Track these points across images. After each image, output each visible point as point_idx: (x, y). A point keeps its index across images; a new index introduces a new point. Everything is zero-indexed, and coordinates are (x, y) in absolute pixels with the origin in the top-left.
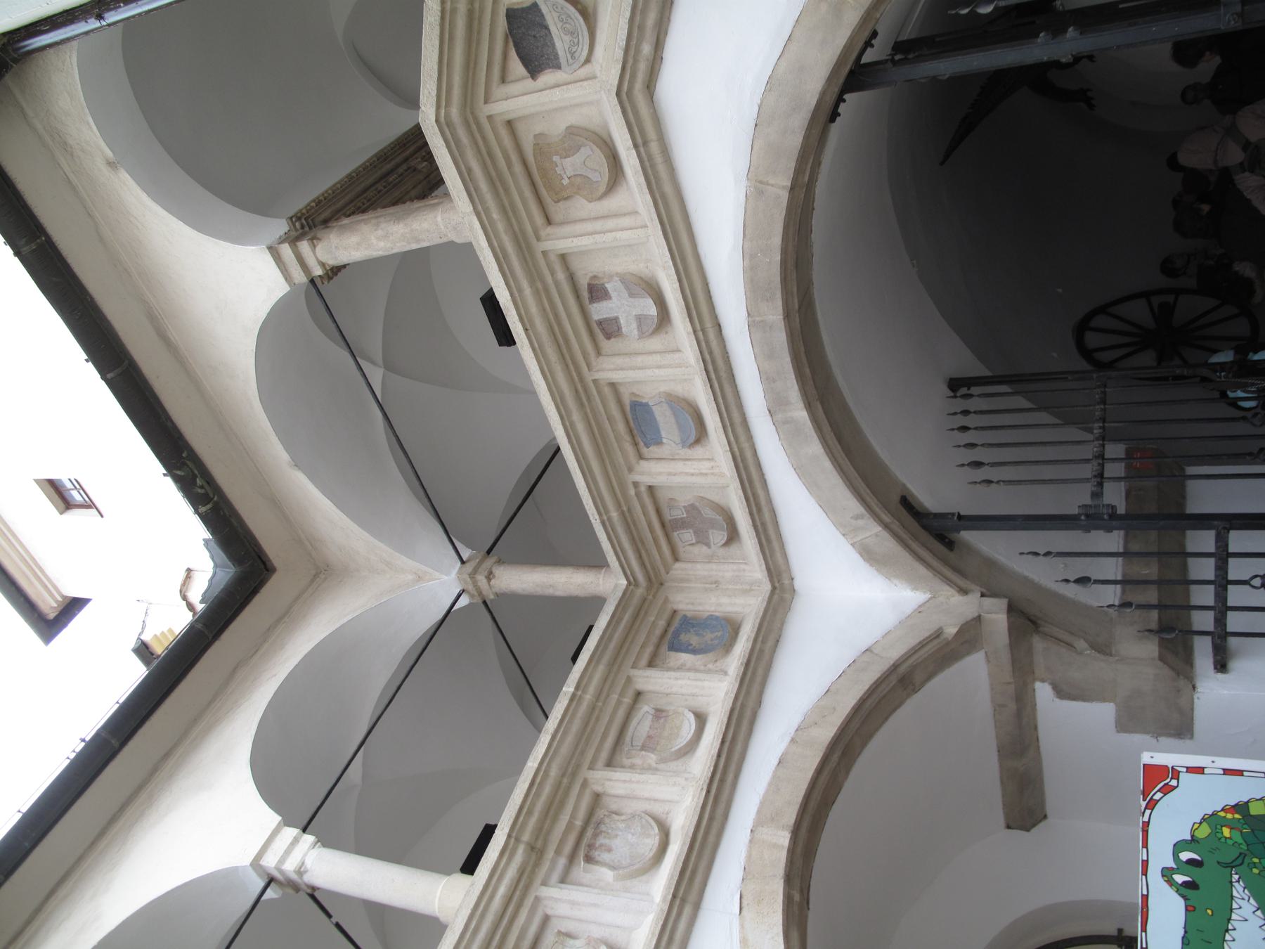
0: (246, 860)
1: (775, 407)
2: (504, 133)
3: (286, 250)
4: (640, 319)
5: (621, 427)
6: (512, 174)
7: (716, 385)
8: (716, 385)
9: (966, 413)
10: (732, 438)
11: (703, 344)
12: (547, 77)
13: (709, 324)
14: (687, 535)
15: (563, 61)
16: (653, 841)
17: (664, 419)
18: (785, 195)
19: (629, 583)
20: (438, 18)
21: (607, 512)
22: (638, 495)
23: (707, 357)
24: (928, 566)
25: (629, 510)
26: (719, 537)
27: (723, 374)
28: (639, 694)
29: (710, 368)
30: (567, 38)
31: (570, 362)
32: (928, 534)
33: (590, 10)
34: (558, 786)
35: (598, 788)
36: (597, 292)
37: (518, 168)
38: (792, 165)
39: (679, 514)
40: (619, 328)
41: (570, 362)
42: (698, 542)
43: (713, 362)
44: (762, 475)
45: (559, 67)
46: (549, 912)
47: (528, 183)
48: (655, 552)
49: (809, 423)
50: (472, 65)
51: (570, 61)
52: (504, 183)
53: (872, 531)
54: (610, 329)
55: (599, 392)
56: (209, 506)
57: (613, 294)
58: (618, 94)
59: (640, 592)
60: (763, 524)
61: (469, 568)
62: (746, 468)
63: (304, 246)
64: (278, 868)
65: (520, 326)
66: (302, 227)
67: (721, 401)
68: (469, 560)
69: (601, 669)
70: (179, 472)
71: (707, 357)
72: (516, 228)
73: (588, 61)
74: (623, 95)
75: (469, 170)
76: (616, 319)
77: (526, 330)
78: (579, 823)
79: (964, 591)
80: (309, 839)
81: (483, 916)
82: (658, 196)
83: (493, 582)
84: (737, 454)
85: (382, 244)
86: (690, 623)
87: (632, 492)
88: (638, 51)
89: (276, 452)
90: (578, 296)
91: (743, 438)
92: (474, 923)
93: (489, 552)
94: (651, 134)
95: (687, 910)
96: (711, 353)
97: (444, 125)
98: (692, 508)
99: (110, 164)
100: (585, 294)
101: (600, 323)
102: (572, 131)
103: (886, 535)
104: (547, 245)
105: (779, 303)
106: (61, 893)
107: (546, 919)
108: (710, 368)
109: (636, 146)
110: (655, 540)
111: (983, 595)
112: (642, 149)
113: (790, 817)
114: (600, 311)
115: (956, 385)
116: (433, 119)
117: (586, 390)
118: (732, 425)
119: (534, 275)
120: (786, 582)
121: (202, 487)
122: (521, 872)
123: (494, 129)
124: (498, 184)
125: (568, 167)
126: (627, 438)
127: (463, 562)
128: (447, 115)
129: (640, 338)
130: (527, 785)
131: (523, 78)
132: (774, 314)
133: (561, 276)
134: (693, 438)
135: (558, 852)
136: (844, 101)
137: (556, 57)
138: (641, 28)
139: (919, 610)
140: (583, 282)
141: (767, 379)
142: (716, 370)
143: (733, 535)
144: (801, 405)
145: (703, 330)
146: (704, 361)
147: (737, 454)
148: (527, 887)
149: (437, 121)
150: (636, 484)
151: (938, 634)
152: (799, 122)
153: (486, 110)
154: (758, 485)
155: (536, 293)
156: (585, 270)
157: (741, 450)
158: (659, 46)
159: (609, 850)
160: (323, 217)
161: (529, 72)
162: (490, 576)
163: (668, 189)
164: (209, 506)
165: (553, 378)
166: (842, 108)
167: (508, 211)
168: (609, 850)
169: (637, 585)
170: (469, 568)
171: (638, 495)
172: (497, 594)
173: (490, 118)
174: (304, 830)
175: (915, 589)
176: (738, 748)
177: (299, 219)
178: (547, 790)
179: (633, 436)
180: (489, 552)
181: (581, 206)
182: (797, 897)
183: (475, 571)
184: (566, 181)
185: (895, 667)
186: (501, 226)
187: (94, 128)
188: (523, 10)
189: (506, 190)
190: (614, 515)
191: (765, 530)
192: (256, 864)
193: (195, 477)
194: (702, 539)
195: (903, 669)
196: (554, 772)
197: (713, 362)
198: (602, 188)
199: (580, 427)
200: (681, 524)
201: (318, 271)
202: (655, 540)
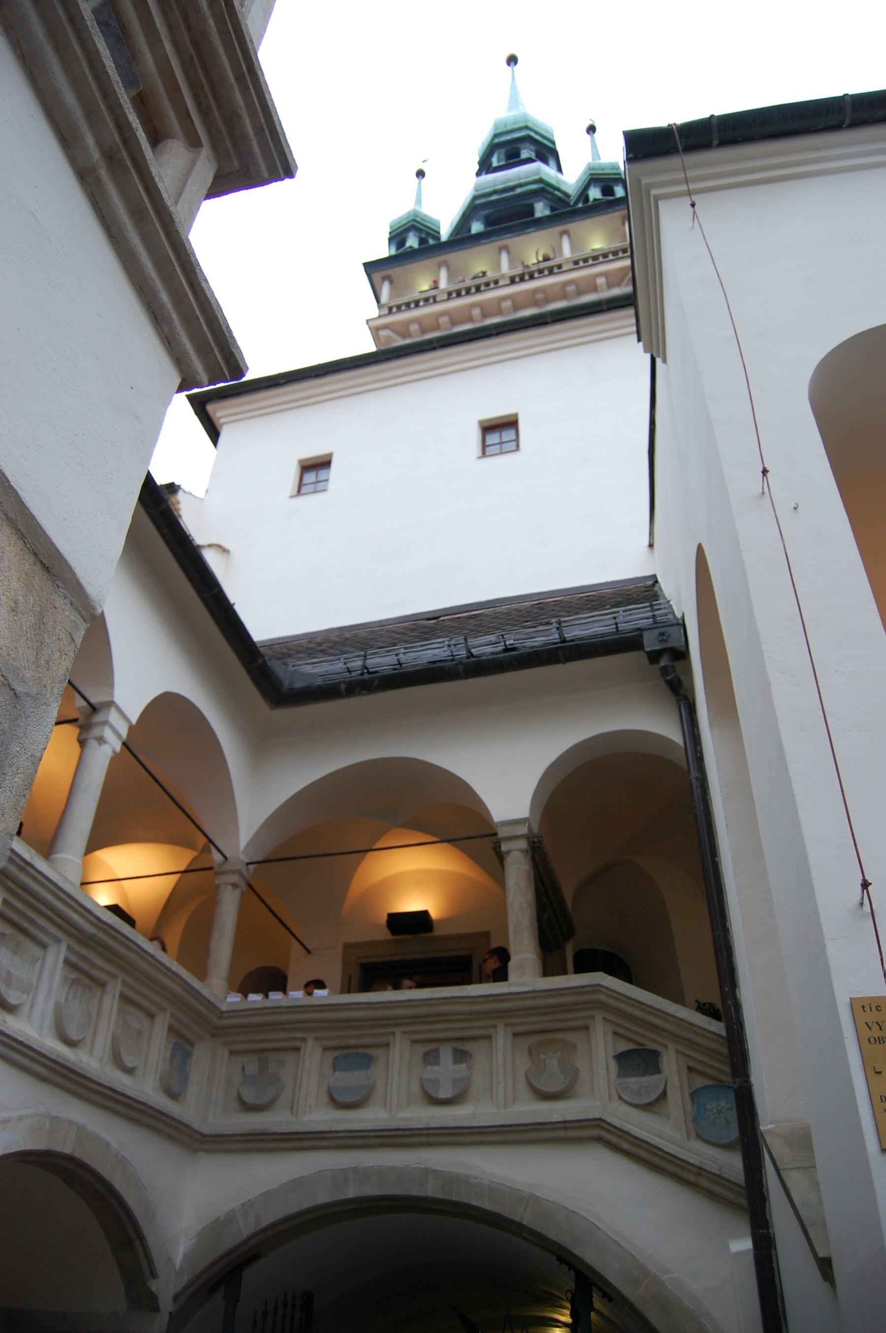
0: (117, 699)
1: (362, 1174)
2: (581, 1023)
3: (523, 830)
4: (436, 1082)
5: (353, 1042)
8: (385, 1133)
9: (294, 1306)
10: (341, 1135)
11: (419, 1132)
12: (613, 1066)
14: (252, 1068)
16: (73, 1033)
17: (355, 1078)
18: (517, 1218)
19: (222, 1012)
20: (663, 1009)
21: (287, 1013)
22: (296, 1039)
23: (408, 1133)
24: (204, 1271)
26: (249, 1096)
28: (152, 1016)
29: (399, 1133)
32: (228, 1272)
35: (109, 987)
36: (461, 1056)
37: (556, 1025)
38: (537, 1228)
43: (402, 1136)
45: (619, 1076)
46: (50, 949)
47: (545, 1028)
49: (343, 1197)
52: (548, 1014)
53: (246, 1228)
54: (431, 1058)
58: (600, 1119)
59: (214, 1019)
60: (262, 1141)
61: (243, 869)
63: (523, 844)
64: (105, 723)
65: (448, 995)
66: (534, 842)
67: (372, 1134)
68: (248, 869)
69: (177, 989)
70: (376, 682)
71: (408, 1133)
73: (620, 1098)
74: (599, 1122)
75: (563, 995)
76: (438, 1064)
77: (445, 998)
78: (94, 972)
79: (176, 1298)
80: (118, 746)
82: (529, 1127)
83: (230, 887)
86: (187, 1055)
88: (625, 1140)
90: (458, 1039)
92: (63, 896)
93: (249, 885)
94: (571, 1134)
95: (45, 1072)
97: (596, 988)
101: (437, 1050)
102: (576, 1072)
103: (239, 1240)
104: (501, 1030)
105: (440, 1196)
107: (44, 947)
108: (399, 1133)
109: (565, 1122)
110: (254, 1041)
111: (171, 1314)
112: (562, 1125)
113: (78, 1155)
114: (446, 1053)
115: (308, 1298)
116: (602, 983)
117: (388, 1025)
118: (351, 1137)
123: (585, 1018)
125: (552, 1061)
126: (343, 1043)
127: (248, 864)
128: (601, 992)
131: (615, 1048)
132: (431, 1190)
133: (476, 1032)
134: (337, 1097)
135: (82, 957)
136: (569, 1270)
137: (626, 1076)
138: (639, 1146)
139: (170, 1260)
140: (467, 1046)
142: (396, 1136)
143: (247, 1107)
145: (428, 1135)
146: (405, 1130)
148: (69, 934)
149: (599, 985)
150: (304, 1040)
151: (154, 1274)
152: (566, 1241)
153: (599, 1016)
156: (478, 1050)
159: (74, 997)
160: (537, 857)
161: (619, 1055)
162: (235, 886)
163: (532, 1135)
166: (565, 1267)
167: (529, 1011)
168: (74, 997)
169: (220, 1018)
170: (243, 869)
171: (296, 1039)
172: (218, 886)
173: (593, 1017)
174: (124, 744)
175: (185, 1255)
177: (540, 842)
178: (123, 951)
179: (342, 1048)
180: (249, 885)
181: (523, 1064)
182: (32, 1159)
183: (241, 874)
184: (542, 1057)
185: (141, 1237)
186: (521, 1004)
188: (658, 1062)
189: (544, 1014)
190: (284, 1018)
192: (111, 704)
195: (137, 1243)
196: (132, 956)
197: (402, 1136)
198: (535, 1083)
201: (504, 847)
202: (254, 1041)
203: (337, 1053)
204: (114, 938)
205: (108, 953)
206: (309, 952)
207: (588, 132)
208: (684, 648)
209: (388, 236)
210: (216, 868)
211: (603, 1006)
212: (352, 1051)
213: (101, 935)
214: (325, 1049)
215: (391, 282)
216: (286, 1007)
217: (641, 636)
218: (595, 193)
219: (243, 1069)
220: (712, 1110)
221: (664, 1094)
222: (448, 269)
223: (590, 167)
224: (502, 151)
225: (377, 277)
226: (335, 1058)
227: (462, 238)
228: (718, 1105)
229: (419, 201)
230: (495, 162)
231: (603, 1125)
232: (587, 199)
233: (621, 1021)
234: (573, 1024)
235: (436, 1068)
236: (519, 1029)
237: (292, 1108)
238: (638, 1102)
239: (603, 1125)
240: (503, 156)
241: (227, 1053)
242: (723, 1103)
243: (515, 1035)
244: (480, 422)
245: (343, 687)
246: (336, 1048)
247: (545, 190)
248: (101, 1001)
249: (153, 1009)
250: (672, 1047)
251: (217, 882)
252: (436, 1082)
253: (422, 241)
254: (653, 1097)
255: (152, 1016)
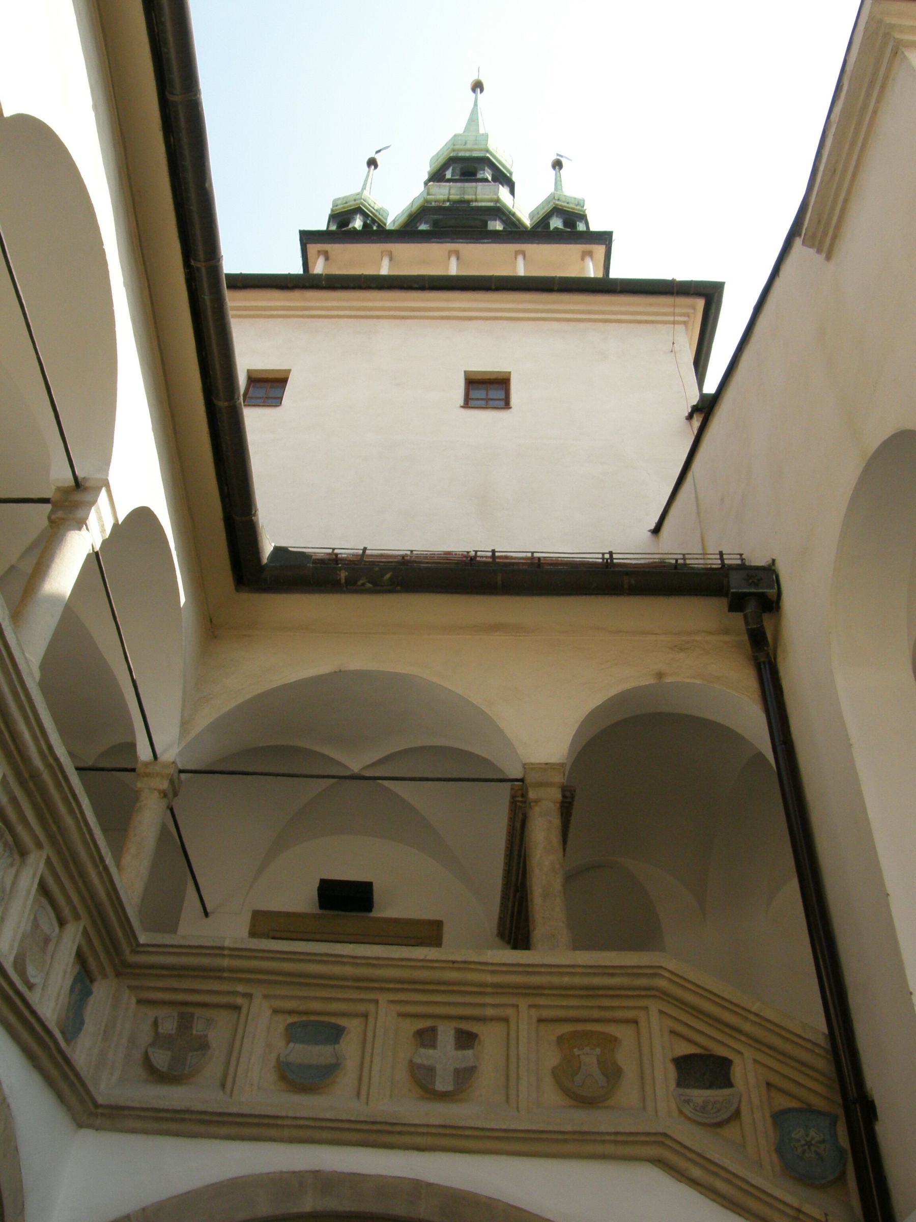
2: (630, 1014)
4: (431, 1070)
5: (316, 1006)
6: (592, 1007)
7: (364, 1127)
8: (364, 1127)
13: (429, 1141)
14: (169, 1026)
15: (681, 1091)
17: (315, 1054)
22: (235, 993)
23: (399, 1129)
25: (220, 978)
27: (372, 1137)
30: (700, 1101)
31: (405, 986)
33: (718, 1130)
34: (57, 820)
35: (32, 858)
37: (596, 1014)
39: (198, 1028)
40: (424, 1046)
41: (405, 986)
42: (157, 1033)
44: (242, 1138)
48: (160, 984)
49: (295, 1210)
50: (694, 1013)
51: (683, 1098)
55: (362, 1000)
56: (343, 581)
57: (460, 1053)
58: (665, 1135)
62: (258, 1125)
70: (388, 576)
72: (547, 992)
74: (662, 1138)
75: (612, 975)
81: (21, 708)
83: (156, 794)
84: (279, 1122)
85: (547, 863)
87: (240, 988)
89: (357, 659)
91: (296, 1133)
96: (400, 1133)
97: (655, 972)
98: (203, 1046)
99: (660, 675)
100: (465, 1026)
101: (433, 1029)
106: (146, 292)
114: (446, 1034)
116: (664, 965)
119: (500, 989)
120: (98, 1122)
121: (363, 585)
122: (25, 759)
124: (591, 993)
127: (181, 771)
129: (411, 1062)
130: (77, 792)
133: (489, 1012)
141: (354, 1180)
144: (319, 1208)
147: (279, 1122)
149: (661, 967)
153: (654, 1006)
154: (233, 1130)
155: (484, 985)
157: (282, 1127)
158: (694, 1183)
163: (570, 1148)
164: (343, 581)
165: (398, 966)
167: (565, 991)
169: (134, 952)
176: (25, 1035)
178: (62, 809)
184: (576, 1051)
187: (688, 680)
190: (226, 962)
191: (173, 1120)
193: (375, 584)
194: (158, 1040)
196: (69, 821)
199: (336, 970)
200: (185, 1022)
201: (532, 795)
202: (175, 990)
203: (290, 1019)
204: (58, 785)
205: (45, 810)
206: (206, 914)
207: (554, 167)
208: (775, 599)
209: (329, 212)
210: (140, 769)
211: (664, 995)
212: (312, 1018)
213: (46, 776)
214: (276, 1011)
215: (327, 259)
216: (230, 949)
217: (727, 576)
218: (556, 223)
219: (156, 1023)
220: (799, 1141)
221: (737, 1114)
222: (391, 259)
223: (552, 197)
224: (459, 167)
225: (312, 248)
226: (292, 1025)
227: (408, 232)
228: (807, 1135)
229: (364, 188)
230: (448, 175)
231: (668, 1142)
232: (548, 225)
233: (684, 1017)
234: (620, 1014)
235: (431, 1052)
236: (546, 1013)
237: (223, 1086)
238: (707, 1121)
239: (668, 1142)
240: (458, 172)
241: (134, 1001)
242: (812, 1133)
243: (540, 1020)
244: (466, 373)
245: (343, 575)
246: (290, 1012)
247: (499, 211)
248: (17, 876)
249: (66, 912)
250: (749, 1054)
251: (139, 785)
252: (431, 1070)
253: (365, 225)
254: (724, 1116)
255: (62, 923)
